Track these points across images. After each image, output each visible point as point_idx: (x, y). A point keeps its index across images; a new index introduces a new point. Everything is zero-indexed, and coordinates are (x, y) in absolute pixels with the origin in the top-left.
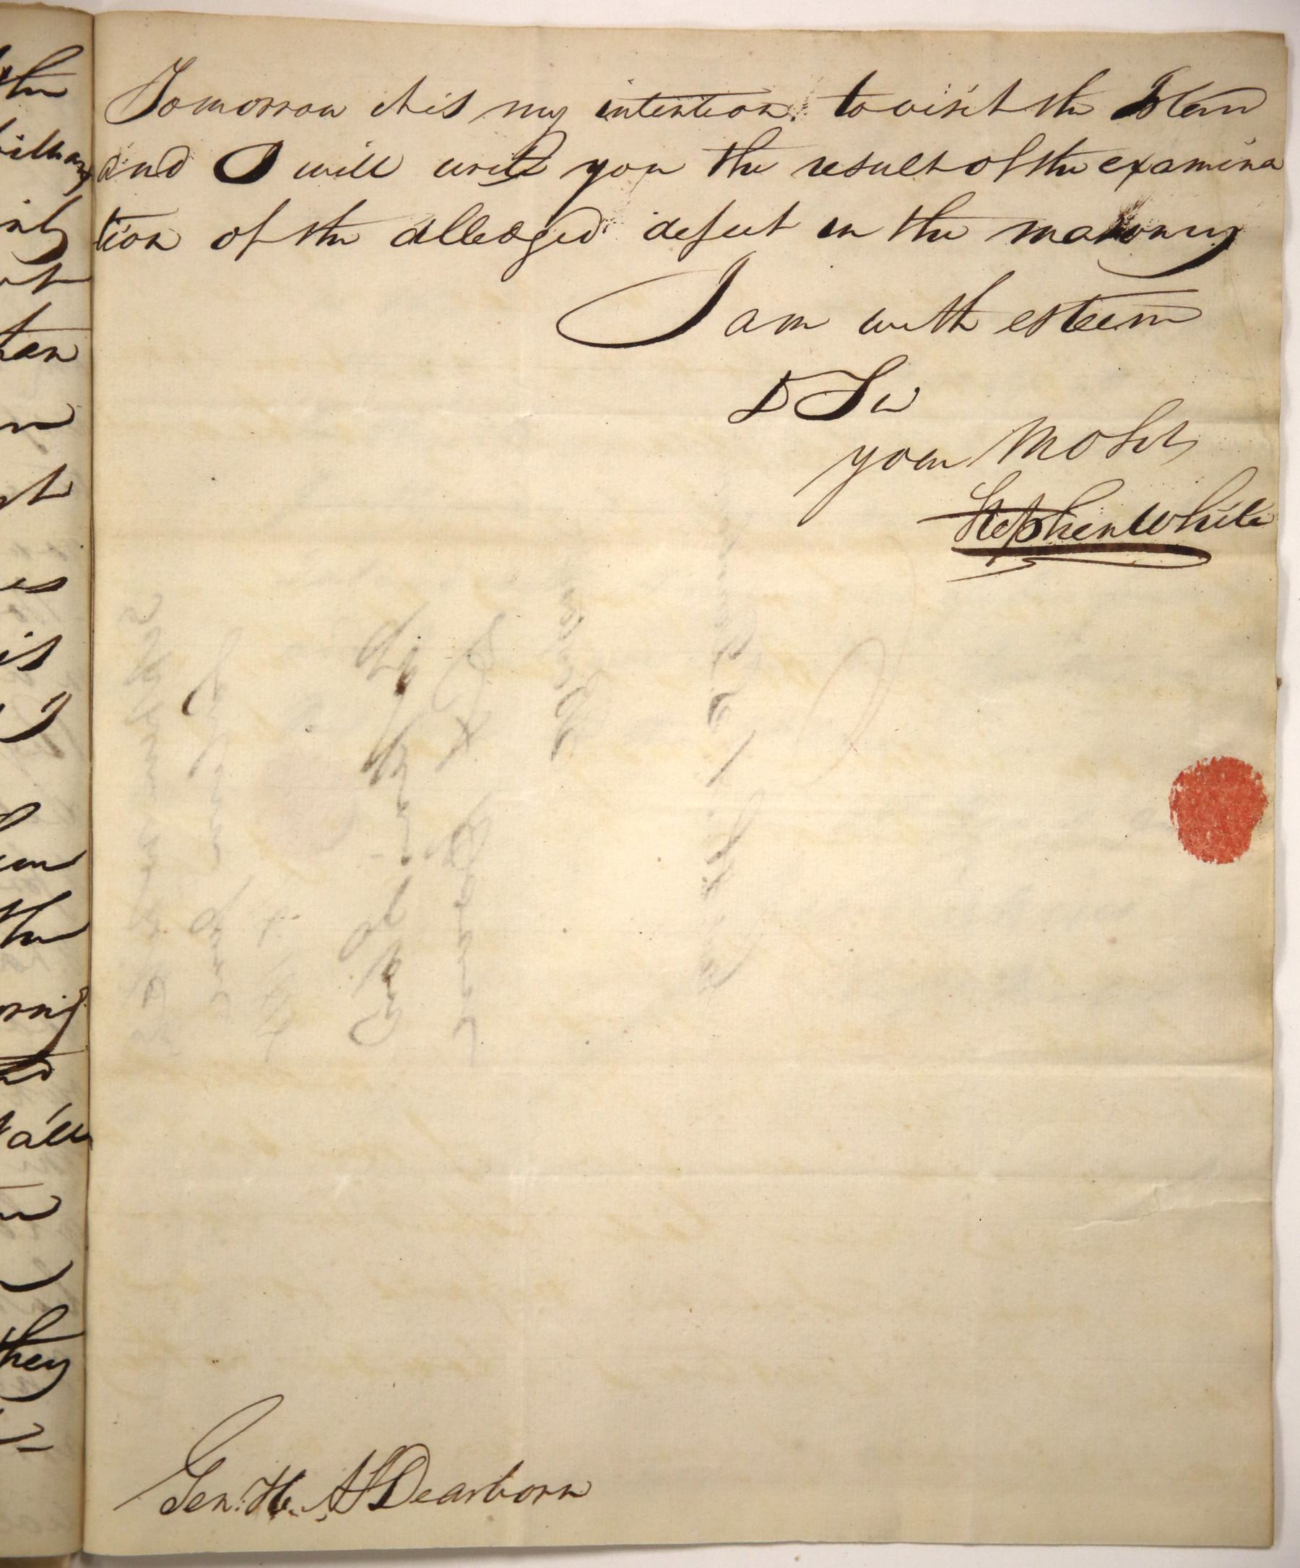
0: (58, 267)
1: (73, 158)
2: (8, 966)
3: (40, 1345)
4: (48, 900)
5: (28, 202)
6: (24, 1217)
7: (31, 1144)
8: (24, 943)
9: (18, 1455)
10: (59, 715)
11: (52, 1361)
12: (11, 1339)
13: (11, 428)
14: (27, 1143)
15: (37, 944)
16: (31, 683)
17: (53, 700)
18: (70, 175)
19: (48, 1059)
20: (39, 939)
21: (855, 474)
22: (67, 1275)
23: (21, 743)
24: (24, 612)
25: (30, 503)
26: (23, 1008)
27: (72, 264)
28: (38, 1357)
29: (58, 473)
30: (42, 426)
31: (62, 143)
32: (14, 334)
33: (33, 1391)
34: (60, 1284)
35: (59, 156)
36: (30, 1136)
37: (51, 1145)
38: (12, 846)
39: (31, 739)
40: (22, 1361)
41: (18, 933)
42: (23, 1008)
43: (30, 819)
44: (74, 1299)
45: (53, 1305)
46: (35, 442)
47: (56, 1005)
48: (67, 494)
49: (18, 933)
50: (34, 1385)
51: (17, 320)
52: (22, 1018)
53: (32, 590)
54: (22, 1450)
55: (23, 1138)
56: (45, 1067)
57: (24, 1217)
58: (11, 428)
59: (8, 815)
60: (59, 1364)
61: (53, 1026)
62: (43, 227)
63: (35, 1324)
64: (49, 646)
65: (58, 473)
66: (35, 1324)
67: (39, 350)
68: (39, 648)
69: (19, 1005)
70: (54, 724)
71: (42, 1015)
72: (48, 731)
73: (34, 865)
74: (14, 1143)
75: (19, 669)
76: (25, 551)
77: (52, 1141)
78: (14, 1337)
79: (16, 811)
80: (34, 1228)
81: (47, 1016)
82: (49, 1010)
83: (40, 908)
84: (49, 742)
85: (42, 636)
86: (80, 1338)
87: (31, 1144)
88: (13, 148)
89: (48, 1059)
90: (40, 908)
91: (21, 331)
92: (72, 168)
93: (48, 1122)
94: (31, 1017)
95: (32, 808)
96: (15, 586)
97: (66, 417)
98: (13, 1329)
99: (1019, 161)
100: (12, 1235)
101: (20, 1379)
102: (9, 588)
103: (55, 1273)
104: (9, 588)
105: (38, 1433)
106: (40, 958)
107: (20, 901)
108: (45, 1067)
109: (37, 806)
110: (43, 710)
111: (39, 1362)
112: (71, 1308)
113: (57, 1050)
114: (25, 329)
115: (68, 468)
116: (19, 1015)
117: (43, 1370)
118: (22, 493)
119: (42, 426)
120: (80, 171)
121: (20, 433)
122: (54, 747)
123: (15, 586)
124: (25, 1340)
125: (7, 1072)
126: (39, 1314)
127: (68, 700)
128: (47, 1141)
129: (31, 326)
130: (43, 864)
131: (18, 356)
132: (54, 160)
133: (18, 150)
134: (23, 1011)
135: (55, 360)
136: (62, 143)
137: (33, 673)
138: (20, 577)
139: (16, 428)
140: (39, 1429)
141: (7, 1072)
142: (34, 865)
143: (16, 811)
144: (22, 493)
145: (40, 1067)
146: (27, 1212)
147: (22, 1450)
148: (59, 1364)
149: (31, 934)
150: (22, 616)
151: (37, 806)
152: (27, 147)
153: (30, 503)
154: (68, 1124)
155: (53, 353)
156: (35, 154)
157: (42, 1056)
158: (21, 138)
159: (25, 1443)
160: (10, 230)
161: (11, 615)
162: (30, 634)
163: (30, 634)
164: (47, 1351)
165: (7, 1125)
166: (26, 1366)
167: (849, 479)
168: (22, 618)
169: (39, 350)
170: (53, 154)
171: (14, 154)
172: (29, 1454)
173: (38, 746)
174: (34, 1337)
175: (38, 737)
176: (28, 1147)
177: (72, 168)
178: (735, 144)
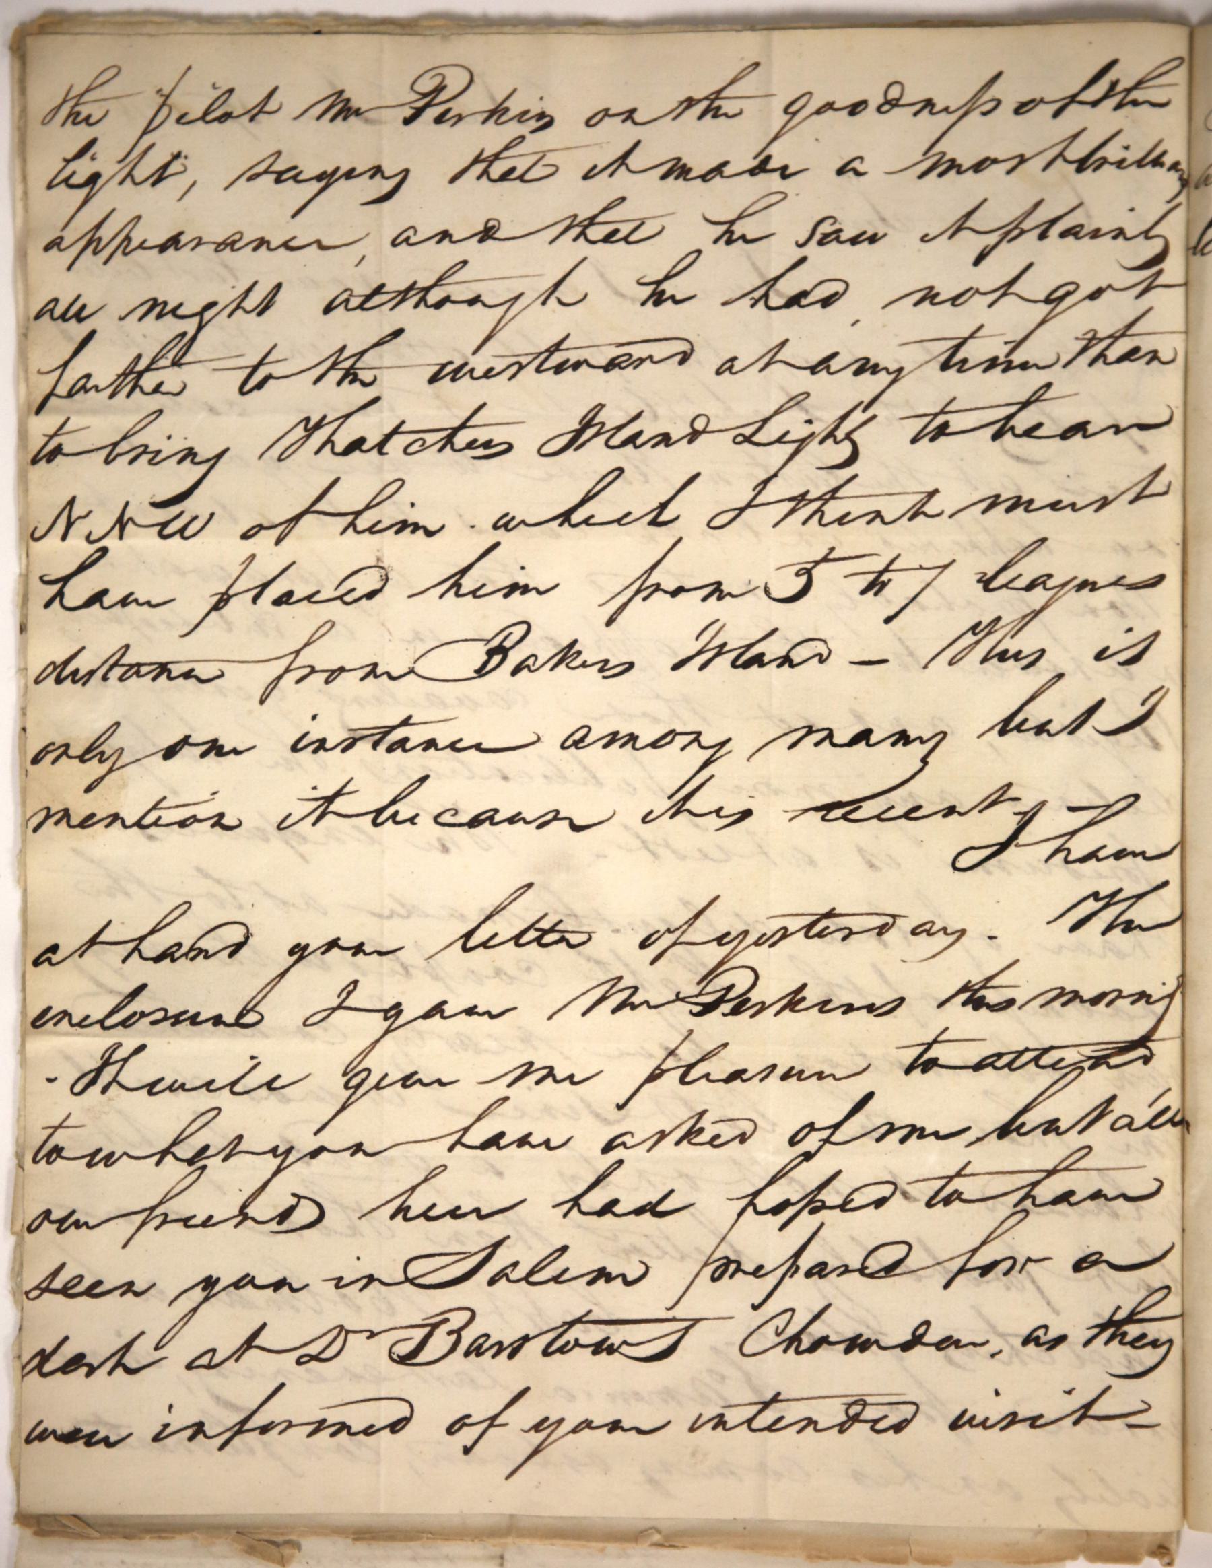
0: (1160, 272)
1: (1175, 166)
2: (1110, 954)
3: (1146, 1325)
4: (1148, 888)
5: (1132, 210)
6: (1128, 1199)
7: (1134, 1127)
8: (1125, 931)
9: (1127, 1432)
10: (1158, 709)
11: (1157, 1340)
12: (1116, 1318)
13: (1113, 430)
14: (1129, 1126)
15: (1137, 932)
16: (1131, 677)
17: (1152, 694)
18: (1171, 182)
19: (1149, 1044)
20: (1140, 927)
21: (278, 1171)
22: (1169, 1256)
23: (1122, 737)
24: (1125, 609)
25: (1131, 502)
26: (1125, 994)
27: (1173, 268)
28: (1144, 1336)
29: (1157, 473)
30: (1143, 427)
31: (1164, 153)
32: (1117, 339)
33: (1140, 1369)
34: (1163, 1266)
35: (1162, 165)
36: (1132, 1119)
37: (1152, 1128)
38: (1112, 836)
39: (1131, 732)
40: (1128, 1339)
41: (1119, 921)
42: (1125, 994)
43: (1130, 810)
44: (1174, 1280)
45: (1157, 1285)
46: (1135, 443)
47: (1156, 992)
48: (1166, 493)
49: (1119, 921)
50: (1141, 1363)
51: (1119, 325)
52: (1123, 1004)
53: (1132, 587)
54: (1130, 1426)
55: (1126, 1121)
56: (1147, 1052)
57: (1128, 1199)
58: (1113, 430)
59: (1109, 806)
60: (1164, 1343)
61: (1154, 1012)
62: (1146, 234)
63: (1140, 1303)
64: (1147, 642)
65: (1157, 473)
66: (1140, 1303)
67: (1141, 354)
68: (1139, 643)
69: (1120, 991)
70: (1153, 718)
71: (1143, 1002)
72: (1147, 724)
73: (1134, 854)
74: (1117, 1126)
75: (1120, 664)
76: (1125, 549)
77: (1154, 1124)
78: (1120, 1315)
79: (1117, 802)
80: (1137, 1209)
81: (1148, 1003)
82: (1150, 996)
83: (1139, 897)
84: (1148, 734)
85: (1141, 632)
86: (1178, 1321)
87: (1134, 1127)
88: (1118, 158)
89: (1149, 1044)
90: (1139, 897)
91: (1123, 335)
92: (1174, 176)
93: (1150, 1106)
94: (1133, 1003)
95: (1132, 799)
96: (1115, 583)
97: (1165, 418)
98: (1119, 1308)
99: (124, 447)
100: (1116, 1215)
101: (1126, 1356)
102: (1110, 585)
103: (1158, 1254)
104: (1110, 585)
105: (1146, 1411)
106: (1140, 946)
107: (1120, 890)
108: (1147, 1052)
109: (1137, 797)
110: (1143, 704)
111: (1145, 1341)
112: (1173, 1289)
113: (1157, 1036)
114: (1129, 332)
115: (1167, 469)
116: (1120, 1002)
117: (1149, 1348)
118: (1123, 493)
119: (1143, 427)
120: (1181, 179)
121: (1122, 435)
122: (1153, 740)
123: (1115, 583)
124: (1131, 1319)
125: (1109, 1056)
126: (1143, 1293)
127: (1166, 693)
128: (1149, 1125)
129: (1133, 330)
130: (1143, 854)
131: (1120, 360)
132: (1158, 169)
133: (1123, 160)
134: (1124, 997)
135: (1156, 363)
136: (1164, 153)
137: (1133, 668)
138: (1121, 574)
139: (1118, 430)
140: (1146, 1407)
141: (1109, 1056)
142: (1134, 854)
143: (1117, 802)
144: (1123, 493)
145: (1142, 1051)
146: (1131, 1193)
147: (1130, 1426)
148: (1164, 1343)
149: (1131, 922)
150: (1122, 613)
151: (1137, 797)
152: (1132, 156)
153: (1131, 502)
154: (1168, 1108)
155: (1154, 356)
156: (1140, 163)
157: (1144, 1041)
158: (1127, 148)
159: (1133, 1420)
160: (1115, 238)
161: (1112, 612)
162: (1130, 630)
163: (1130, 630)
164: (1153, 1330)
165: (1110, 1108)
166: (1132, 1344)
167: (269, 1181)
168: (1123, 614)
169: (1141, 354)
170: (1157, 162)
171: (1120, 164)
172: (1137, 1430)
173: (1137, 738)
174: (1139, 1316)
175: (1137, 730)
176: (1130, 1129)
177: (1174, 176)
178: (383, 286)
